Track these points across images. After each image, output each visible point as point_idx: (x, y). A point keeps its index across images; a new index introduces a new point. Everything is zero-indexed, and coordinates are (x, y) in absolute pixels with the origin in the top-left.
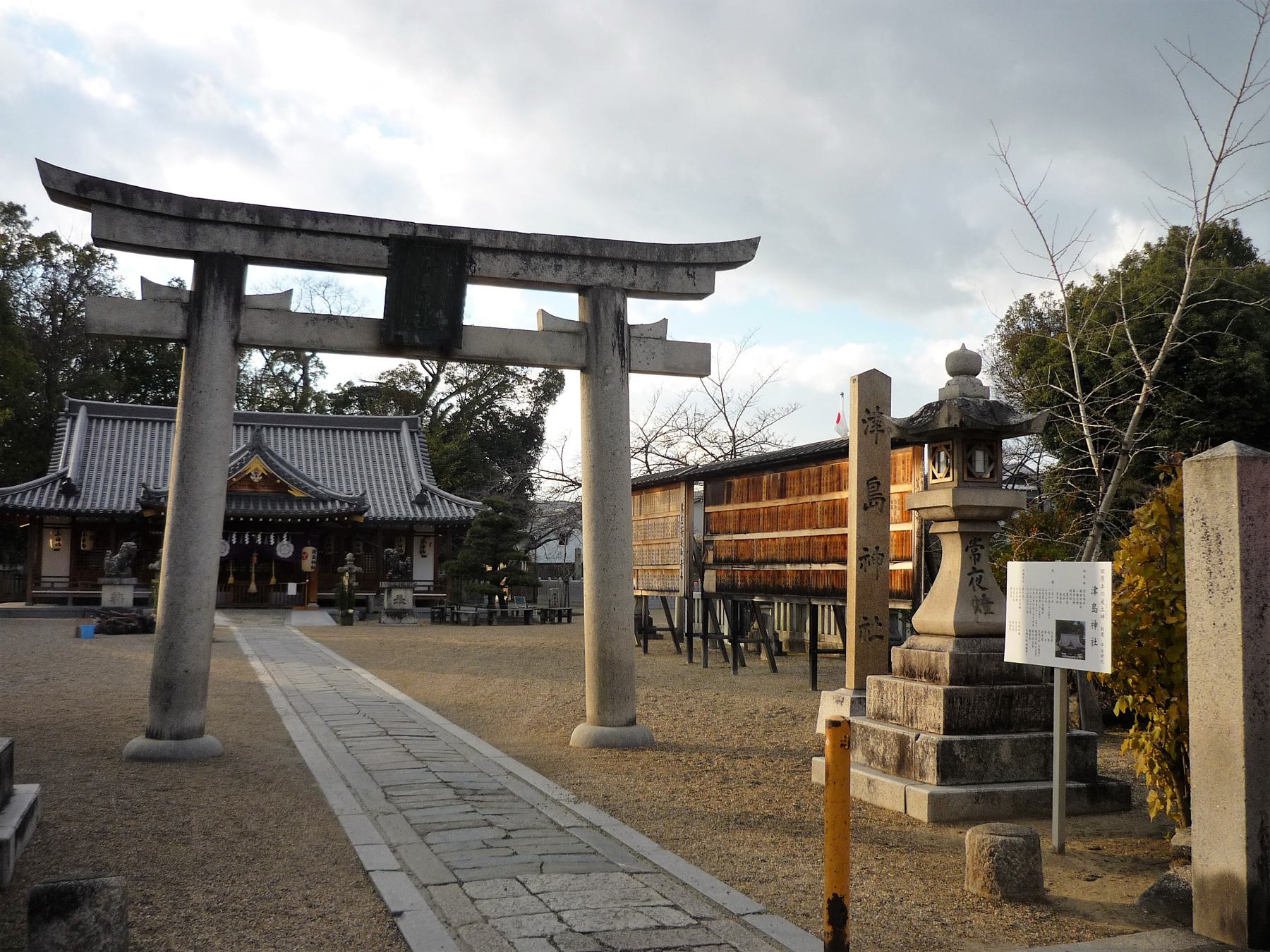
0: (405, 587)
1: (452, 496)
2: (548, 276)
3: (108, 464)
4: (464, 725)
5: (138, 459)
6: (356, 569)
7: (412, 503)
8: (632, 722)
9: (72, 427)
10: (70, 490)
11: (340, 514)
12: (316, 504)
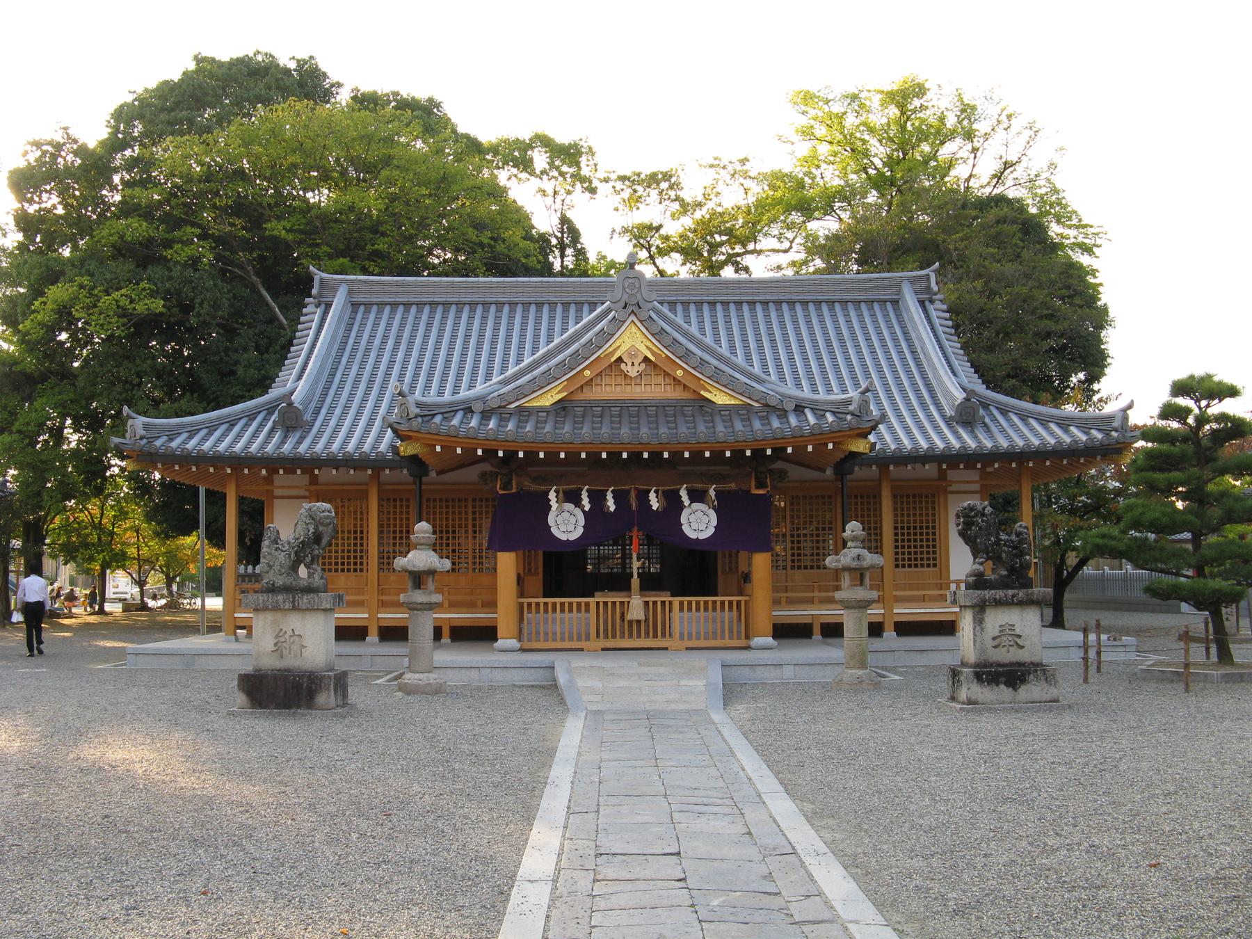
0: (1022, 604)
3: (373, 375)
5: (425, 367)
7: (948, 421)
10: (292, 420)
11: (819, 438)
12: (765, 420)
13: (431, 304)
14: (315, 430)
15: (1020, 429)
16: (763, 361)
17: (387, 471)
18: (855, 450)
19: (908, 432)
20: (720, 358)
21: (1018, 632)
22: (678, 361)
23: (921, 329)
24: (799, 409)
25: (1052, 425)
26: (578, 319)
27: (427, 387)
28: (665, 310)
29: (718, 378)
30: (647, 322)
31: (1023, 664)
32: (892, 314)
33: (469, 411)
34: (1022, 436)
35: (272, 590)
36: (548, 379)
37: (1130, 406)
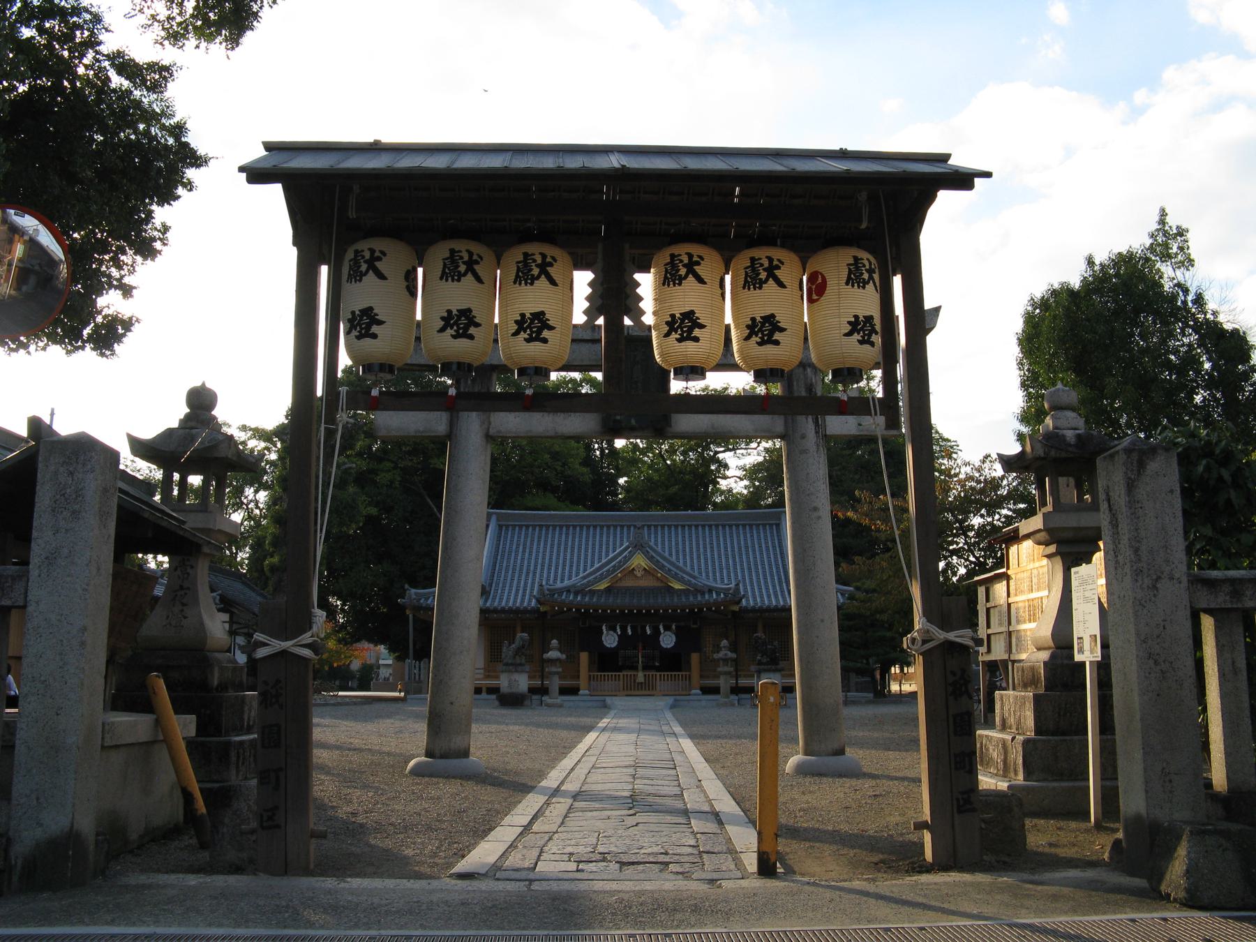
3: (515, 566)
8: (840, 752)
11: (716, 603)
12: (695, 596)
20: (678, 568)
24: (710, 591)
29: (676, 577)
30: (646, 554)
35: (507, 664)
36: (602, 578)
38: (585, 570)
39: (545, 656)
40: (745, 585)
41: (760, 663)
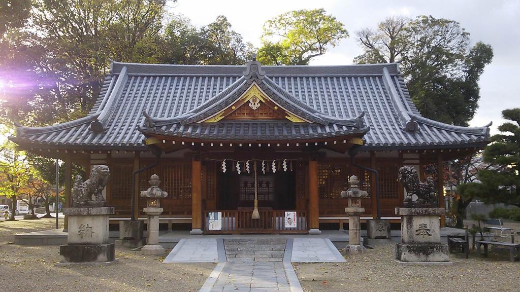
0: (429, 215)
1: (441, 124)
2: (244, 232)
4: (213, 64)
6: (361, 193)
7: (403, 131)
9: (115, 83)
10: (98, 128)
11: (339, 137)
12: (315, 129)
13: (172, 76)
14: (108, 133)
15: (437, 134)
16: (318, 103)
17: (142, 152)
18: (356, 143)
19: (384, 135)
21: (428, 228)
22: (275, 102)
23: (392, 89)
25: (443, 131)
26: (227, 85)
27: (163, 112)
28: (273, 81)
30: (261, 85)
31: (432, 243)
32: (378, 82)
33: (179, 125)
34: (439, 138)
36: (213, 112)
37: (491, 124)
38: (199, 103)
39: (145, 210)
40: (369, 118)
41: (410, 204)
